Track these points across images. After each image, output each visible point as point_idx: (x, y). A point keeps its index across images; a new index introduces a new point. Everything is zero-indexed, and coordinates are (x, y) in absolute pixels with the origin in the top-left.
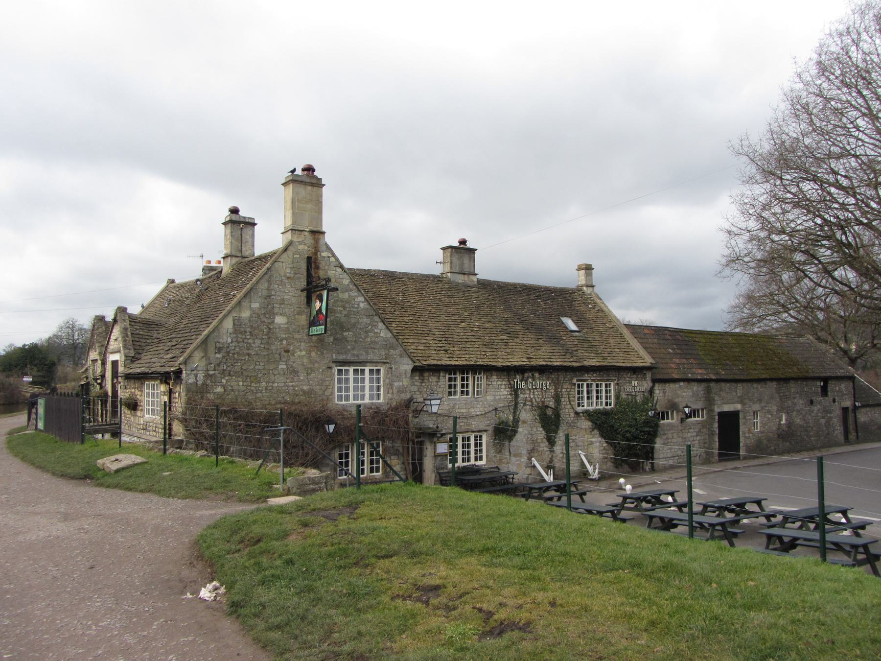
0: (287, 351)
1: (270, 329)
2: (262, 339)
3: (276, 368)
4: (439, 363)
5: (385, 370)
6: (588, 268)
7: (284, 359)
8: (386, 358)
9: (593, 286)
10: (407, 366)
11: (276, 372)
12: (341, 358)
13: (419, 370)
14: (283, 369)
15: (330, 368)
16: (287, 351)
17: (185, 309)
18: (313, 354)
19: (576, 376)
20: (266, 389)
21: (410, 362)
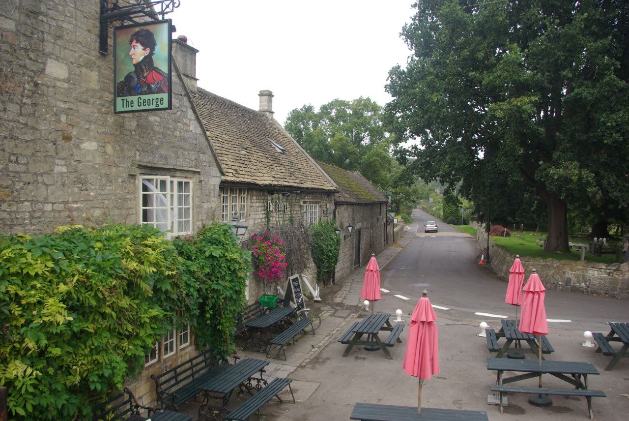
0: (67, 138)
1: (36, 85)
2: (22, 105)
3: (50, 172)
4: (322, 187)
5: (195, 184)
6: (270, 95)
7: (63, 154)
8: (196, 167)
9: (273, 113)
10: (215, 181)
11: (47, 179)
12: (147, 160)
13: (226, 187)
14: (61, 173)
15: (133, 176)
16: (67, 138)
17: (95, 231)
18: (109, 149)
19: (302, 198)
20: (32, 217)
21: (219, 174)
